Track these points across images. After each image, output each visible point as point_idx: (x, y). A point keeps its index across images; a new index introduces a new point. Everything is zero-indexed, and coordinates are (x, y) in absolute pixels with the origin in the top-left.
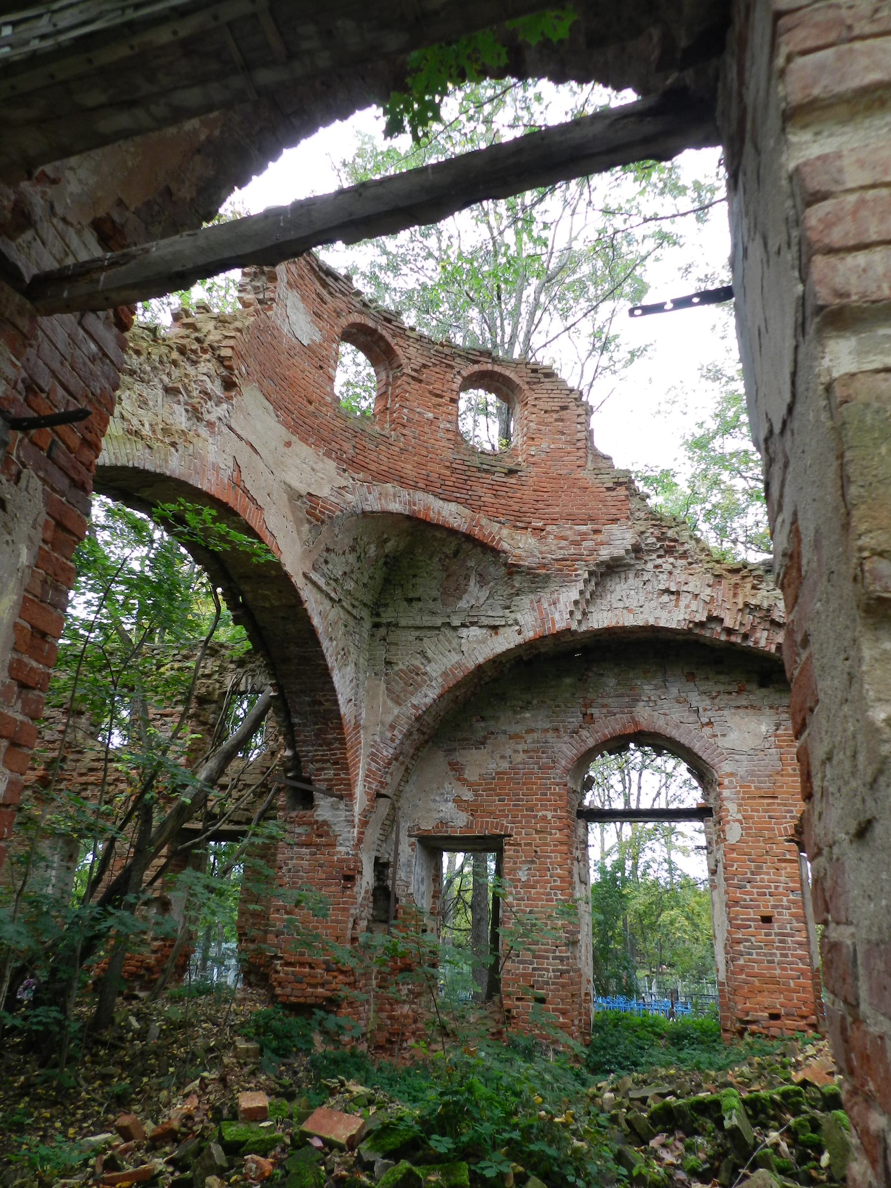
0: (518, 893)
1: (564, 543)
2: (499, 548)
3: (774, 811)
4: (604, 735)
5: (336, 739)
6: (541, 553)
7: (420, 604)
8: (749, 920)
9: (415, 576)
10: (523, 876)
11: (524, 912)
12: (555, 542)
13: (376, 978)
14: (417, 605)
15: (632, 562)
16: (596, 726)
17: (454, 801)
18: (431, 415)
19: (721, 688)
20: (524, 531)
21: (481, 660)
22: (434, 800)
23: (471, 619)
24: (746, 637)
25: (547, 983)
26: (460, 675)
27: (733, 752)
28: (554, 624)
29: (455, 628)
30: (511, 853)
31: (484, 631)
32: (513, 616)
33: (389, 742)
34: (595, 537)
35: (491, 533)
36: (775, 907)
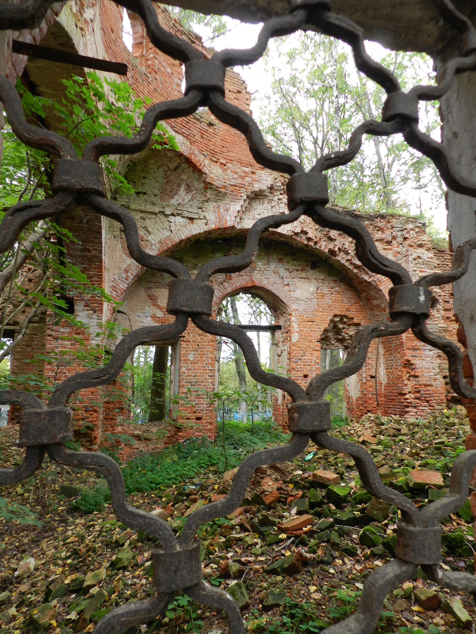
0: (188, 366)
1: (236, 176)
2: (203, 171)
3: (313, 328)
4: (237, 286)
5: (96, 275)
6: (224, 179)
7: (146, 197)
8: (299, 377)
9: (144, 178)
10: (191, 357)
11: (191, 376)
12: (232, 174)
13: (103, 414)
14: (143, 197)
15: (268, 194)
16: (232, 281)
17: (151, 317)
18: (169, 70)
19: (295, 268)
20: (216, 164)
21: (183, 237)
22: (139, 316)
23: (178, 212)
24: (316, 243)
25: (203, 410)
26: (170, 244)
27: (297, 299)
28: (226, 222)
29: (167, 216)
30: (185, 345)
31: (185, 220)
32: (203, 213)
33: (124, 280)
34: (252, 176)
35: (199, 160)
36: (310, 371)
